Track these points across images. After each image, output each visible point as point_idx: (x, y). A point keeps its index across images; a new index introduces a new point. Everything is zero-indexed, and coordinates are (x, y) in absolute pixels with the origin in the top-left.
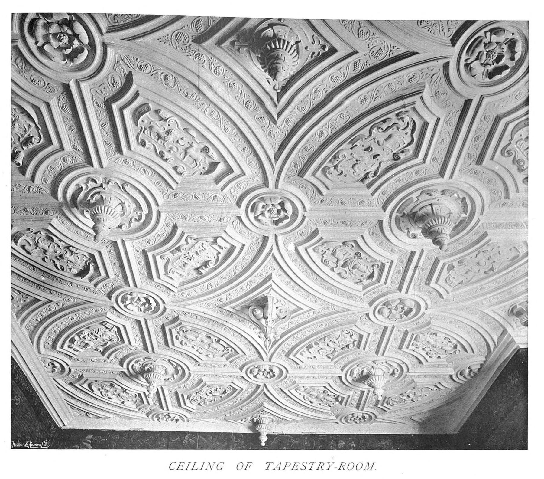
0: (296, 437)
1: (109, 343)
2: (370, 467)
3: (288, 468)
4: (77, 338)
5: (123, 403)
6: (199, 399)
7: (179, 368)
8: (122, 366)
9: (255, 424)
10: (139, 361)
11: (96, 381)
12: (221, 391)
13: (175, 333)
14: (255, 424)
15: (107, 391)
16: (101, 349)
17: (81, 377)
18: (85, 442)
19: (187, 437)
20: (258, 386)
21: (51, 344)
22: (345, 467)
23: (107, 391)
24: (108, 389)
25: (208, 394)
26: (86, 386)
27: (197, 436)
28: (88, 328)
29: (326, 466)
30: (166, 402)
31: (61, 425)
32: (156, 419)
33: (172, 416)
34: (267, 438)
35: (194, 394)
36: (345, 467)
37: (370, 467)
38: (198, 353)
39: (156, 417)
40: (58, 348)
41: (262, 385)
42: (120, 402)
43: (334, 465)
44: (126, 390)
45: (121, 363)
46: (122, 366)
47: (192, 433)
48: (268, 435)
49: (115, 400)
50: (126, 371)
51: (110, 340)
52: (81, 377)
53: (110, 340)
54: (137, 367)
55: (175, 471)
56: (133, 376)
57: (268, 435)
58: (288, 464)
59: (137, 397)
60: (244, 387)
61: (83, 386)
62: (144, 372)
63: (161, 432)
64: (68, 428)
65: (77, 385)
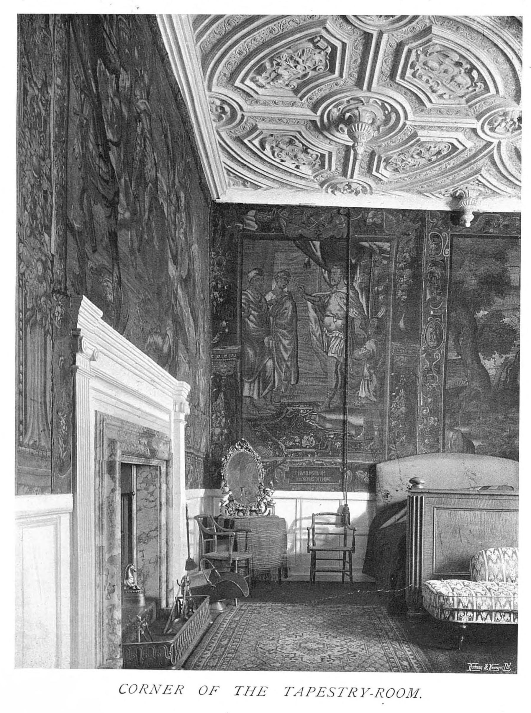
0: (506, 216)
1: (311, 74)
2: (414, 694)
3: (312, 695)
4: (268, 65)
5: (297, 167)
6: (399, 163)
7: (393, 116)
8: (315, 111)
9: (457, 198)
10: (340, 104)
11: (272, 135)
12: (434, 150)
13: (413, 58)
14: (457, 198)
15: (282, 150)
16: (295, 84)
17: (254, 128)
18: (248, 219)
19: (370, 215)
20: (490, 143)
21: (228, 75)
22: (384, 694)
23: (282, 150)
24: (284, 147)
25: (415, 156)
26: (256, 142)
27: (383, 214)
28: (290, 48)
29: (359, 693)
30: (233, 150)
31: (215, 197)
32: (330, 190)
33: (354, 186)
34: (473, 217)
35: (395, 156)
36: (384, 694)
37: (414, 694)
38: (430, 91)
39: (332, 188)
40: (237, 83)
41: (496, 142)
42: (293, 166)
43: (370, 691)
44: (307, 148)
45: (315, 108)
46: (315, 111)
47: (376, 209)
48: (474, 213)
49: (289, 164)
50: (318, 120)
51: (315, 69)
52: (254, 128)
53: (315, 69)
54: (336, 113)
55: (148, 694)
56: (321, 128)
57: (474, 213)
58: (312, 689)
59: (318, 160)
60: (469, 144)
61: (253, 142)
62: (348, 121)
63: (339, 209)
64: (224, 202)
65: (246, 141)
